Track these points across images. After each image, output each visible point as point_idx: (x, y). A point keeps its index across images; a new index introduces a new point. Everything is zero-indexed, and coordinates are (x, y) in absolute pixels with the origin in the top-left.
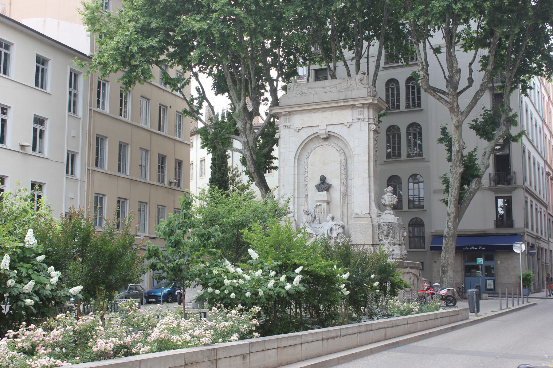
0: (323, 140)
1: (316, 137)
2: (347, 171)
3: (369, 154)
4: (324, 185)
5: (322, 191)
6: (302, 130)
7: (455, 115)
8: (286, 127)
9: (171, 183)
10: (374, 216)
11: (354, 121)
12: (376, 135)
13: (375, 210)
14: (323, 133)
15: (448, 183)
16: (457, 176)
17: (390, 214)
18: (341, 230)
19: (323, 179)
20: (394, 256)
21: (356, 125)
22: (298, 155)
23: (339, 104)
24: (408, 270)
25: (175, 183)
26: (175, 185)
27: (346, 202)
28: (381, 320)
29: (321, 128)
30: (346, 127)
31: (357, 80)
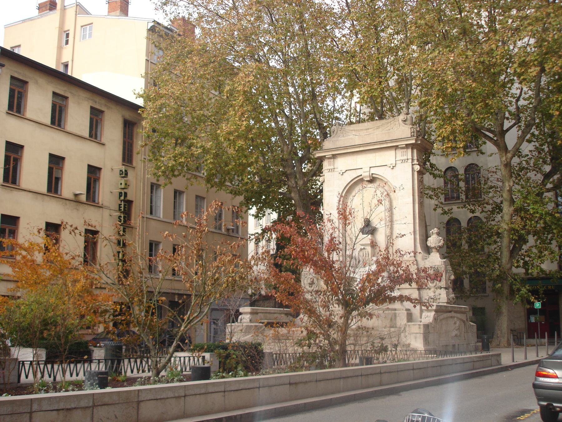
0: (367, 183)
1: (359, 181)
8: (330, 170)
9: (228, 230)
11: (397, 162)
12: (421, 176)
14: (366, 175)
19: (368, 223)
24: (453, 314)
25: (233, 230)
26: (233, 232)
28: (304, 372)
29: (364, 170)
31: (400, 121)
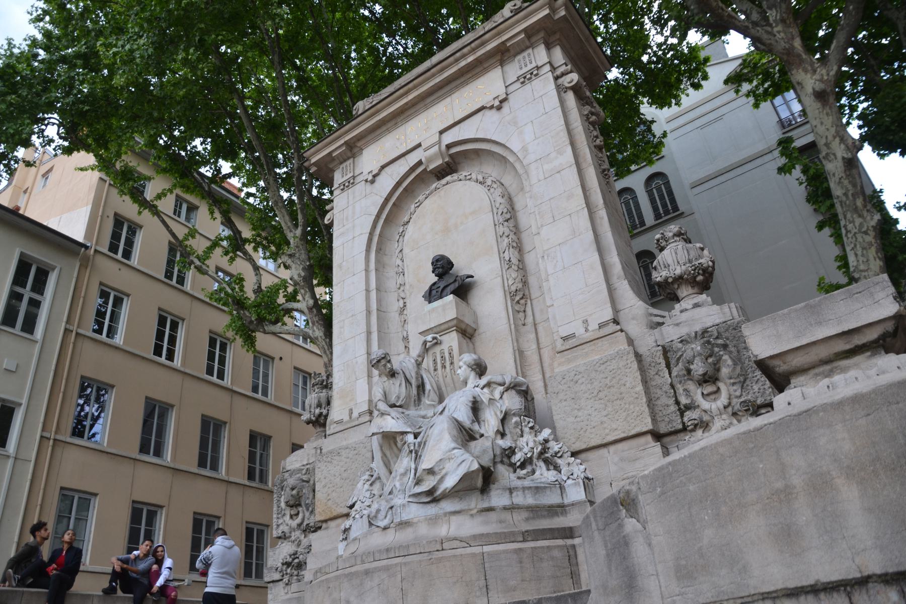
2: (516, 226)
3: (573, 144)
4: (449, 281)
5: (441, 297)
6: (383, 173)
7: (806, 71)
10: (636, 328)
13: (633, 305)
16: (869, 239)
17: (696, 306)
18: (513, 402)
19: (442, 266)
22: (375, 239)
23: (463, 63)
27: (530, 319)
30: (494, 111)
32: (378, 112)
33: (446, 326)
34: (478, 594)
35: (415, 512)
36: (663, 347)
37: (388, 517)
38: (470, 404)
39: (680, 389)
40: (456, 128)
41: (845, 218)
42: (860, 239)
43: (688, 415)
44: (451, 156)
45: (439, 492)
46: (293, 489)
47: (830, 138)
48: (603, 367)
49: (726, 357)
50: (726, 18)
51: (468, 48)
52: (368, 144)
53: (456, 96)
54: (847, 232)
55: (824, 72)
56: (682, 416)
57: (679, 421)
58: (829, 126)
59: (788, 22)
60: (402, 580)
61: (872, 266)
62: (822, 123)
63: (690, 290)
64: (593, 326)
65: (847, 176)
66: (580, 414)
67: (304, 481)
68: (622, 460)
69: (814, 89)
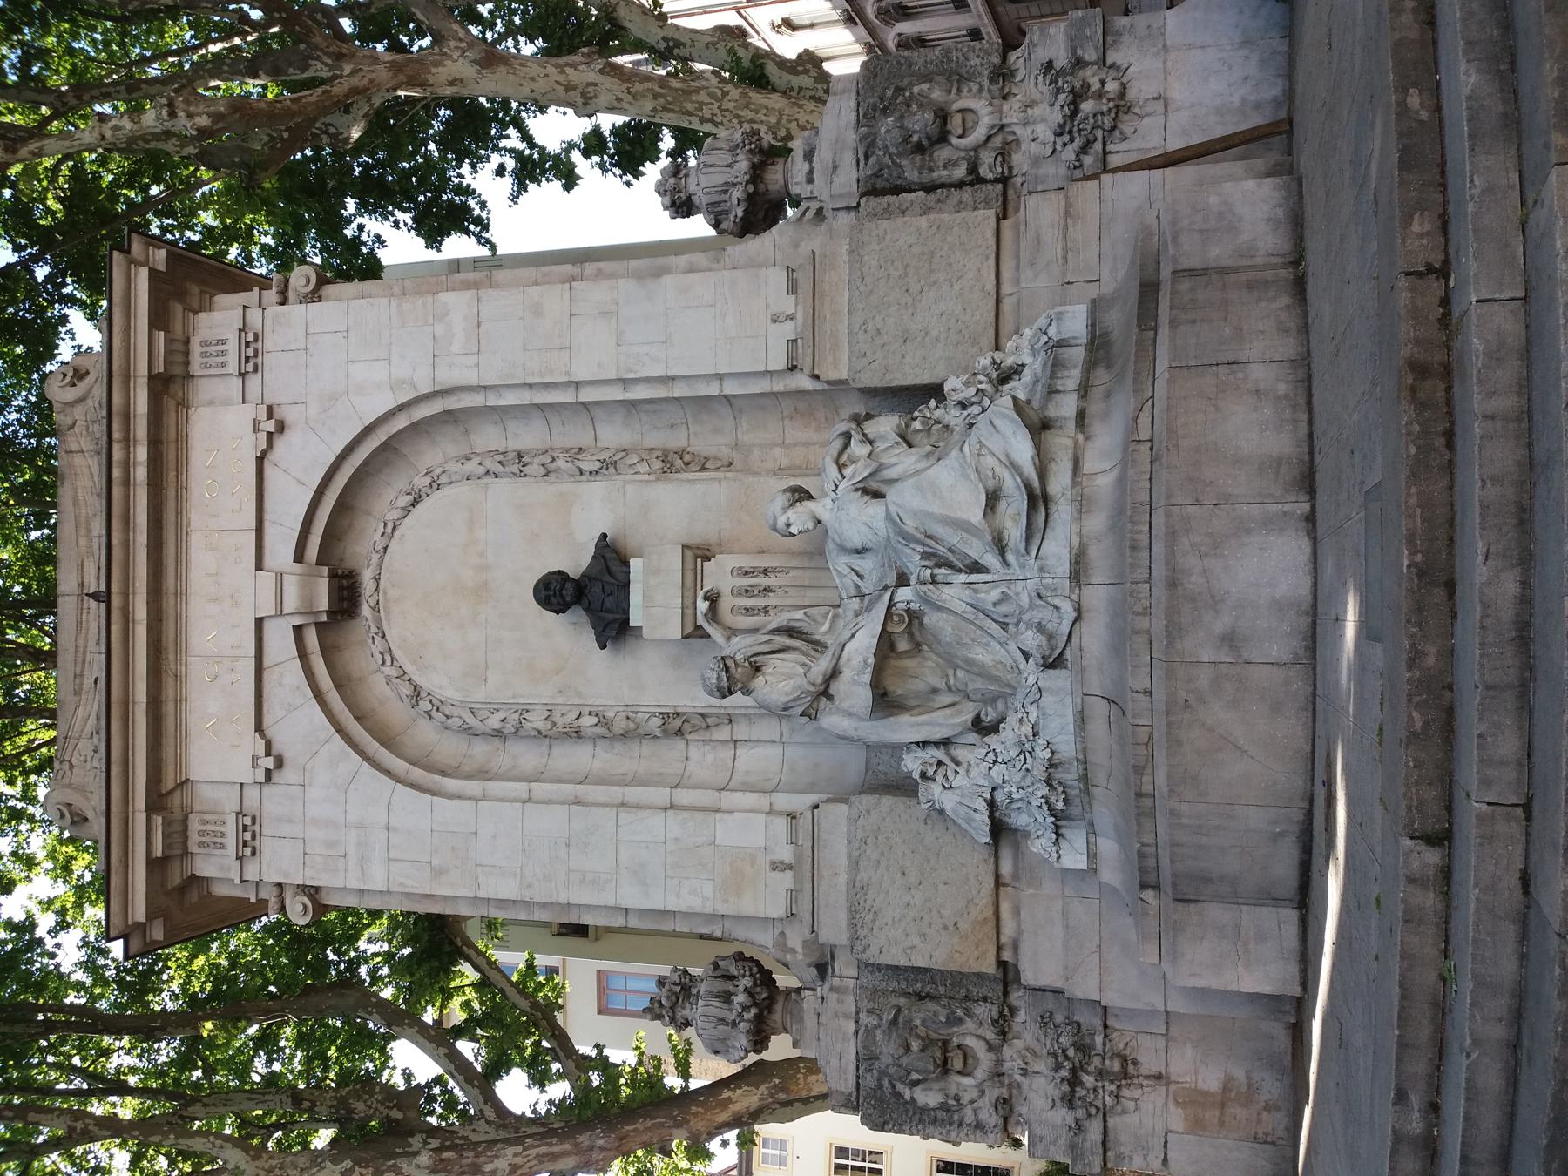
4: (593, 594)
7: (437, 64)
8: (249, 846)
15: (727, 183)
19: (556, 593)
20: (1090, 55)
21: (281, 378)
23: (141, 473)
30: (279, 443)
32: (126, 703)
33: (689, 575)
34: (1241, 375)
35: (1057, 548)
36: (863, 195)
37: (1057, 602)
38: (867, 498)
39: (941, 174)
40: (269, 530)
41: (691, 114)
42: (731, 105)
43: (984, 171)
44: (320, 562)
45: (1036, 483)
46: (908, 1049)
47: (561, 78)
48: (868, 280)
49: (916, 90)
50: (294, 107)
51: (116, 448)
52: (181, 762)
53: (196, 518)
54: (711, 121)
55: (453, 44)
56: (983, 181)
57: (990, 187)
58: (542, 72)
59: (345, 51)
60: (1198, 503)
61: (777, 106)
62: (533, 79)
63: (779, 167)
64: (788, 304)
65: (628, 81)
66: (934, 333)
67: (895, 1021)
68: (1032, 264)
69: (475, 62)
